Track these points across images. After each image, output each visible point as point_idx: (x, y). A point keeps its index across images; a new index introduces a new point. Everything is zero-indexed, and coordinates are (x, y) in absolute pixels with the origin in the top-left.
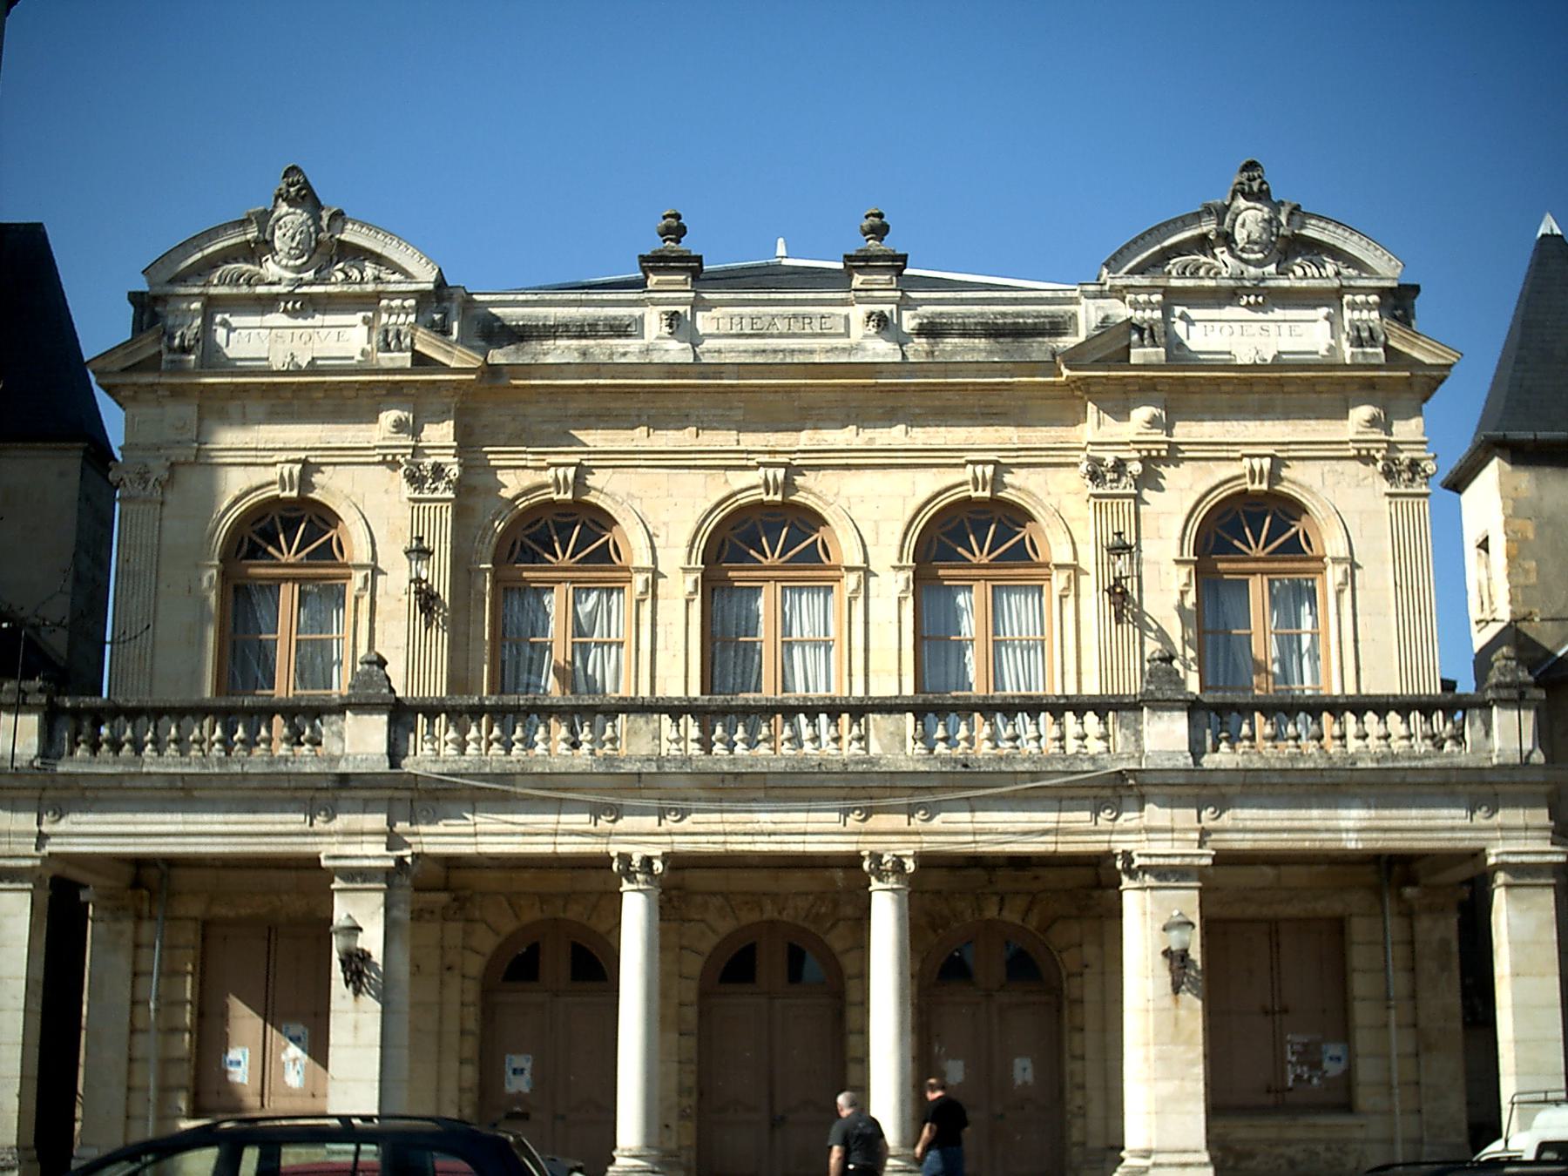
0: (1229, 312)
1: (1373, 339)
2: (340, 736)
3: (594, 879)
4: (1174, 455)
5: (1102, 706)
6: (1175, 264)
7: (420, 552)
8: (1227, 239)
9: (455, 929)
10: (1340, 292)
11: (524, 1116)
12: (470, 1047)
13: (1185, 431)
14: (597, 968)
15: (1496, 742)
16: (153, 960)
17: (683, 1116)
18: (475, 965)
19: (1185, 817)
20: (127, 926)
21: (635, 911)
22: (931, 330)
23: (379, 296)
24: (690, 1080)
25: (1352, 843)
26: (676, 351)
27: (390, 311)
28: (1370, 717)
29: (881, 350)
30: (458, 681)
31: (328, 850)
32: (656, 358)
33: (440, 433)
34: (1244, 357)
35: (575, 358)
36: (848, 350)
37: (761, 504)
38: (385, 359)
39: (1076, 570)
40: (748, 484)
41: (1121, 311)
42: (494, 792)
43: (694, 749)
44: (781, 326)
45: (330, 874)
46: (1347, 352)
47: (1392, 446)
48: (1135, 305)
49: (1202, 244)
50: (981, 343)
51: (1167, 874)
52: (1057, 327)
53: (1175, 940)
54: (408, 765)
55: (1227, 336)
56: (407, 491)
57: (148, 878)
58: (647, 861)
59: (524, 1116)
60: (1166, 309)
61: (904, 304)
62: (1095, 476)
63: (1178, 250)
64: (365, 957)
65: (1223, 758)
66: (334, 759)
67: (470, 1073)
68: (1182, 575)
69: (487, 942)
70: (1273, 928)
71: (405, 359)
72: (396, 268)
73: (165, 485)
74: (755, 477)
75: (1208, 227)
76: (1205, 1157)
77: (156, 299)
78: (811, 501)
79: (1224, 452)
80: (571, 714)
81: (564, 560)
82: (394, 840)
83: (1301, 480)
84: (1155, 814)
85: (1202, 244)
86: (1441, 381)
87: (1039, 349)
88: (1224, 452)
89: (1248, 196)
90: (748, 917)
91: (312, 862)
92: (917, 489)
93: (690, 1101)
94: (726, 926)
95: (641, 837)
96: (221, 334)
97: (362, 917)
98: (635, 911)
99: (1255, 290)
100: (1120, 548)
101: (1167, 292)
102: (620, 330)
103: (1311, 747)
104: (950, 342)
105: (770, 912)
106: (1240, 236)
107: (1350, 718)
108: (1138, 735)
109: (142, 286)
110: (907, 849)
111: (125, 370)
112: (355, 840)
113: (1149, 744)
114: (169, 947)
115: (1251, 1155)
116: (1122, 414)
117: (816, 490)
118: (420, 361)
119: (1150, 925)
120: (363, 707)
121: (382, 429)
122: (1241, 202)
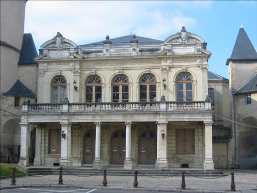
0: (180, 47)
1: (200, 51)
2: (62, 108)
3: (122, 125)
4: (173, 67)
5: (200, 102)
6: (174, 41)
7: (75, 82)
8: (180, 37)
9: (80, 131)
10: (196, 44)
11: (89, 154)
12: (82, 145)
13: (174, 64)
14: (124, 135)
15: (206, 107)
16: (43, 134)
17: (108, 154)
18: (82, 135)
19: (165, 117)
20: (40, 130)
21: (98, 130)
22: (141, 51)
23: (69, 49)
24: (109, 149)
25: (186, 120)
26: (108, 54)
27: (198, 46)
28: (199, 104)
29: (134, 54)
30: (80, 99)
31: (61, 122)
32: (105, 56)
33: (78, 67)
34: (183, 53)
35: (95, 56)
36: (130, 54)
37: (119, 75)
38: (70, 57)
39: (160, 82)
40: (117, 72)
41: (166, 48)
42: (80, 114)
43: (110, 109)
44: (122, 51)
45: (61, 125)
46: (197, 53)
47: (202, 65)
48: (168, 47)
49: (177, 38)
50: (148, 52)
51: (163, 124)
52: (158, 50)
53: (163, 132)
54: (168, 110)
55: (180, 51)
56: (73, 74)
57: (42, 125)
58: (129, 123)
59: (89, 154)
60: (172, 47)
61: (137, 47)
62: (162, 70)
63: (174, 39)
64: (65, 134)
65: (170, 109)
66: (62, 111)
67: (82, 149)
68: (174, 83)
69: (84, 132)
70: (185, 130)
71: (73, 57)
72: (72, 45)
73: (44, 74)
74: (118, 71)
75: (178, 36)
76: (212, 162)
77: (42, 50)
78: (189, 72)
79: (180, 66)
80: (187, 103)
81: (121, 82)
82: (68, 120)
83: (190, 70)
84: (161, 117)
85: (177, 38)
86: (210, 56)
87: (155, 53)
88: (180, 66)
89: (183, 31)
90: (117, 129)
91: (59, 123)
92: (139, 73)
93: (109, 152)
94: (114, 130)
95: (129, 120)
96: (174, 50)
97: (65, 130)
98: (98, 130)
99: (185, 44)
100: (164, 80)
101: (172, 45)
102: (101, 52)
103: (182, 108)
104: (144, 52)
105: (119, 128)
106: (182, 37)
107: (196, 104)
108: (160, 106)
109: (40, 48)
110: (130, 121)
111: (39, 60)
112: (64, 121)
113: (161, 108)
114: (45, 133)
115: (180, 160)
116: (166, 62)
117: (127, 73)
118: (75, 57)
119: (161, 130)
120: (65, 104)
121: (198, 62)
122: (182, 32)
